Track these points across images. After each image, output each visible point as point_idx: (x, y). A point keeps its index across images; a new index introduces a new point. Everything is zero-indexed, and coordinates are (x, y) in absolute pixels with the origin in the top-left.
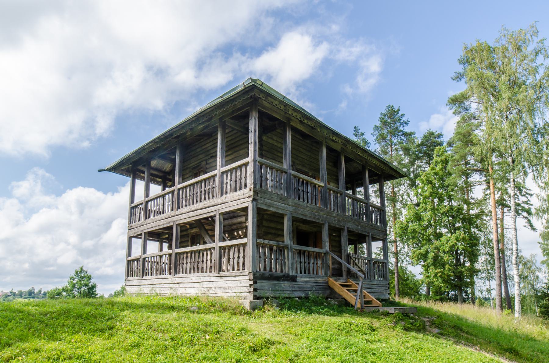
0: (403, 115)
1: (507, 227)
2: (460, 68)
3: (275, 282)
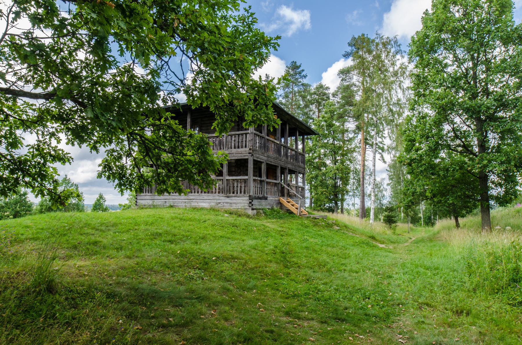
0: (303, 71)
1: (367, 158)
2: (349, 49)
3: (260, 200)
